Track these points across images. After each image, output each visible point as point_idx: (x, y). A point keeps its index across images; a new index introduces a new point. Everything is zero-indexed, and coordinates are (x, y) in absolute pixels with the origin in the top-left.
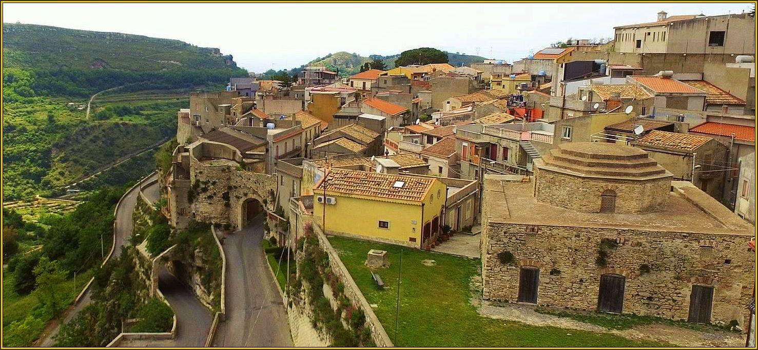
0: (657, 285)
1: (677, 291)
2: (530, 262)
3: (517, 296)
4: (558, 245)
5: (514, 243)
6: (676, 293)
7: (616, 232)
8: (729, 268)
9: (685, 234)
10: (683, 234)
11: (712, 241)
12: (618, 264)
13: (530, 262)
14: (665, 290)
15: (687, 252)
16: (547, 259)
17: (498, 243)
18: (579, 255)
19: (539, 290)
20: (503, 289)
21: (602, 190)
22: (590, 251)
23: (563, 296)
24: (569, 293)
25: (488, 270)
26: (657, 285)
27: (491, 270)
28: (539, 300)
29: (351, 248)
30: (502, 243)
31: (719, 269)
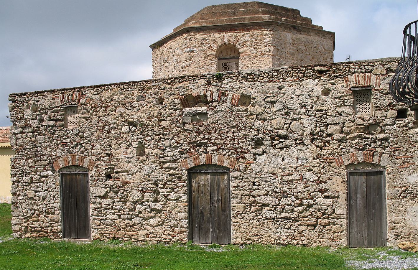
0: (285, 178)
1: (322, 186)
2: (73, 158)
3: (60, 227)
6: (320, 191)
7: (203, 81)
8: (406, 126)
9: (320, 68)
10: (316, 68)
11: (369, 74)
12: (214, 145)
13: (73, 158)
14: (300, 186)
15: (329, 102)
18: (148, 135)
21: (215, 47)
22: (163, 123)
26: (285, 178)
27: (19, 182)
28: (94, 233)
30: (30, 130)
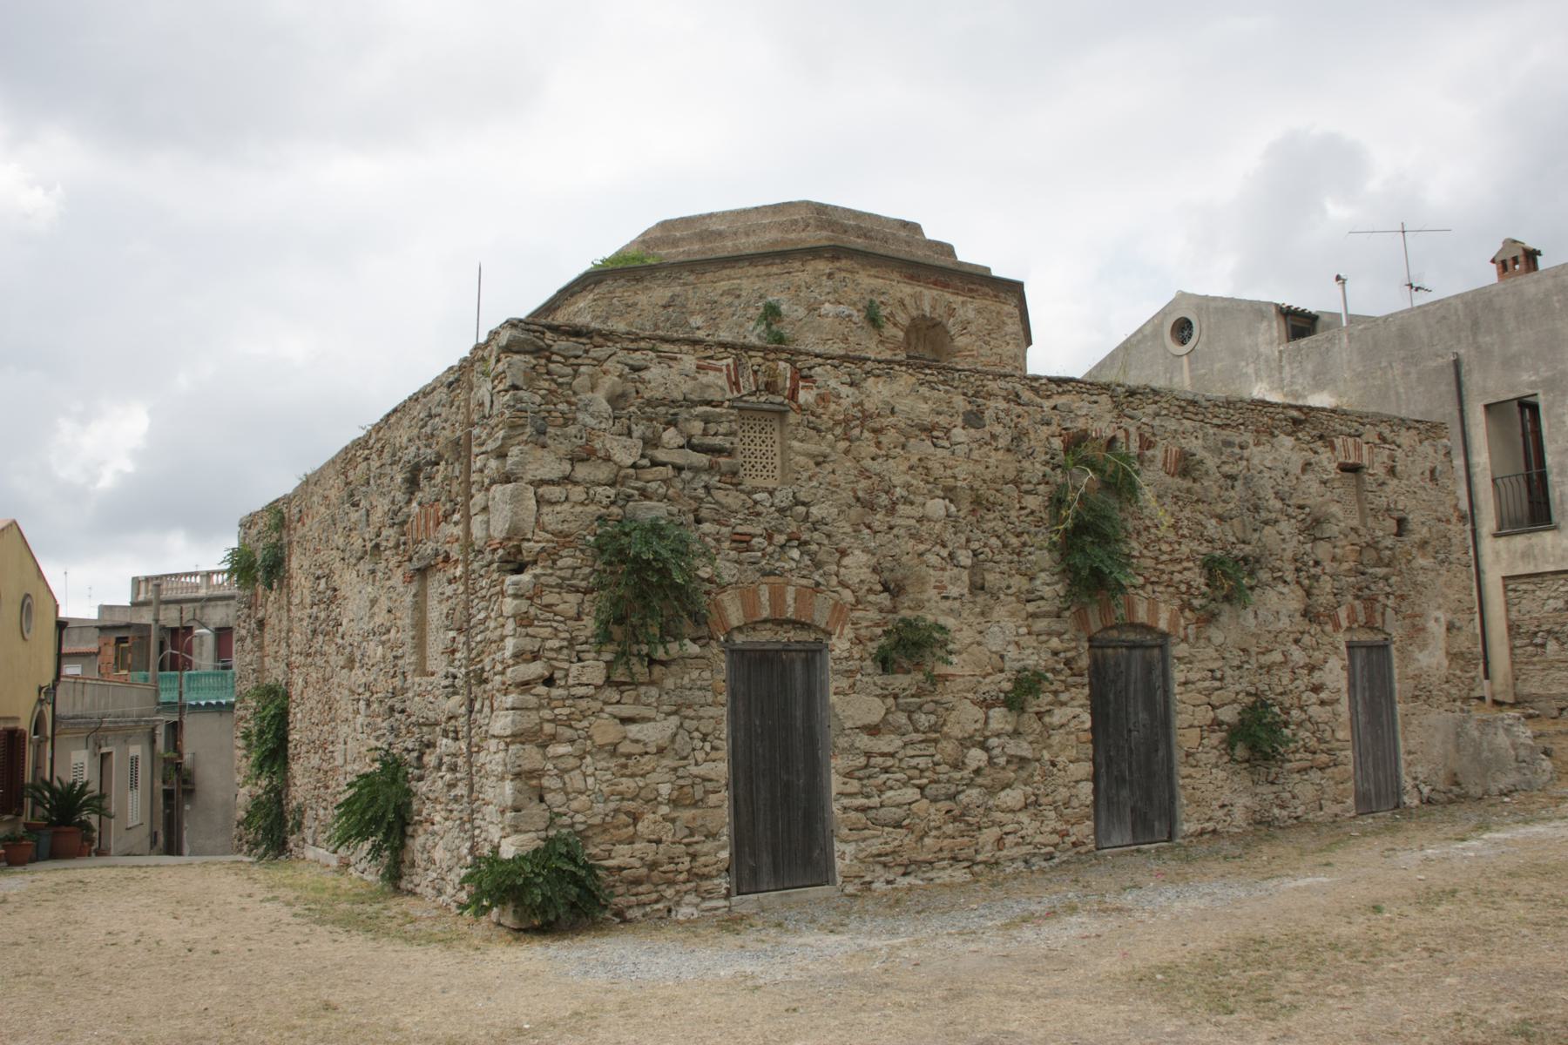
2: (777, 597)
4: (897, 472)
5: (679, 469)
13: (777, 597)
16: (857, 566)
17: (582, 471)
19: (836, 783)
20: (636, 818)
23: (952, 797)
24: (978, 771)
25: (525, 686)
29: (1536, 645)
31: (1155, 570)
